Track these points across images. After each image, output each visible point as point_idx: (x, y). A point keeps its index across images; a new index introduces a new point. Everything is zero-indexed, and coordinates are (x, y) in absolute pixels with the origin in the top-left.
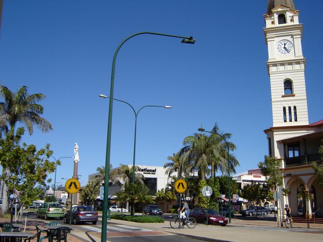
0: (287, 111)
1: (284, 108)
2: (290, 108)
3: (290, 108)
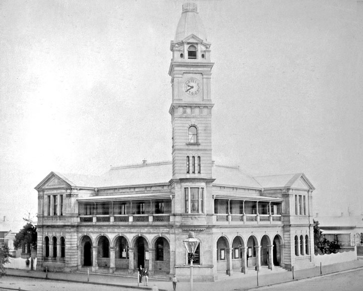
1: (188, 157)
2: (55, 239)
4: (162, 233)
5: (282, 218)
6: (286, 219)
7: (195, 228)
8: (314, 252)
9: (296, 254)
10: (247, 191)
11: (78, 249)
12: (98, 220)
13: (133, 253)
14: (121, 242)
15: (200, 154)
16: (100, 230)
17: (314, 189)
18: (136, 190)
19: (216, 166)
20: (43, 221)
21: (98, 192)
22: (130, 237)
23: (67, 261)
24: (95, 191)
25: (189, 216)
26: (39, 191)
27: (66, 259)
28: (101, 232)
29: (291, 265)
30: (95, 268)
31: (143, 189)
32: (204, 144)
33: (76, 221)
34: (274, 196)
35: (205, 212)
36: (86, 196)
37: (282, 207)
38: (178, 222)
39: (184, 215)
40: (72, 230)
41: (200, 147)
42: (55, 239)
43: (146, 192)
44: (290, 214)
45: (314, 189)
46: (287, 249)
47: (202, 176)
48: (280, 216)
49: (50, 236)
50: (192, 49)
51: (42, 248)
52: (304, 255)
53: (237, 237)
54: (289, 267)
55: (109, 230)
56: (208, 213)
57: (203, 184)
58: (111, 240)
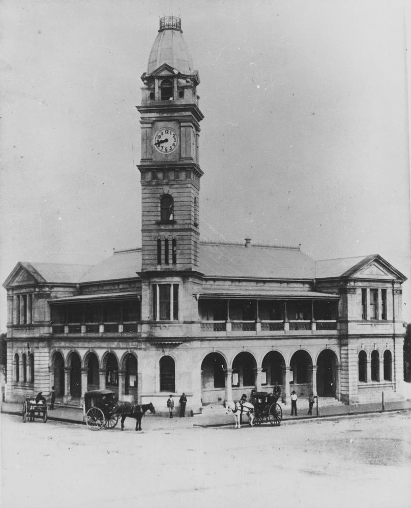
2: (24, 355)
4: (131, 348)
5: (339, 325)
6: (344, 326)
7: (171, 341)
8: (403, 378)
9: (362, 377)
10: (285, 285)
11: (50, 372)
12: (319, 327)
13: (86, 378)
14: (301, 358)
15: (175, 235)
16: (72, 345)
17: (405, 278)
18: (121, 286)
19: (253, 246)
20: (12, 333)
21: (84, 288)
22: (100, 353)
23: (37, 388)
24: (77, 288)
25: (158, 325)
26: (8, 290)
27: (35, 386)
28: (72, 347)
29: (348, 396)
30: (67, 399)
31: (127, 286)
32: (181, 222)
33: (45, 331)
34: (330, 290)
35: (181, 318)
36: (62, 295)
37: (339, 309)
38: (144, 333)
39: (152, 323)
40: (41, 345)
41: (176, 227)
42: (375, 354)
43: (130, 289)
44: (349, 319)
45: (405, 278)
46: (343, 372)
47: (179, 267)
48: (335, 321)
49: (20, 352)
50: (167, 86)
51: (12, 371)
52: (378, 381)
53: (385, 351)
54: (346, 398)
55: (80, 344)
56: (186, 320)
57: (177, 280)
58: (229, 362)
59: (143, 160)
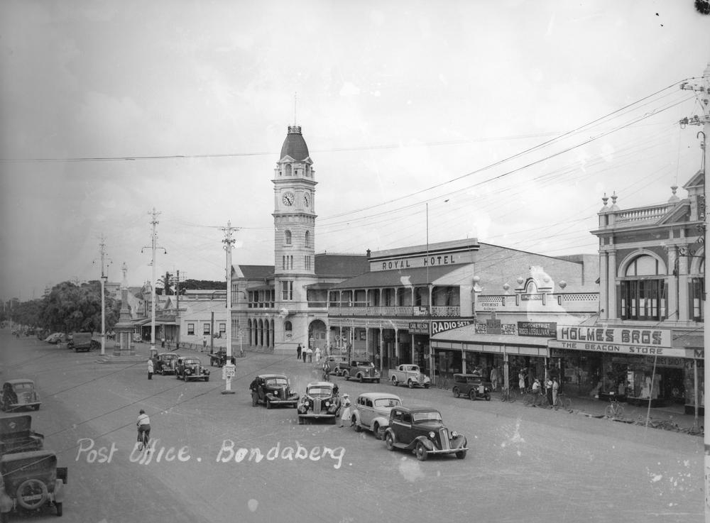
0: (286, 260)
1: (284, 257)
2: (288, 257)
3: (288, 257)
59: (276, 211)
